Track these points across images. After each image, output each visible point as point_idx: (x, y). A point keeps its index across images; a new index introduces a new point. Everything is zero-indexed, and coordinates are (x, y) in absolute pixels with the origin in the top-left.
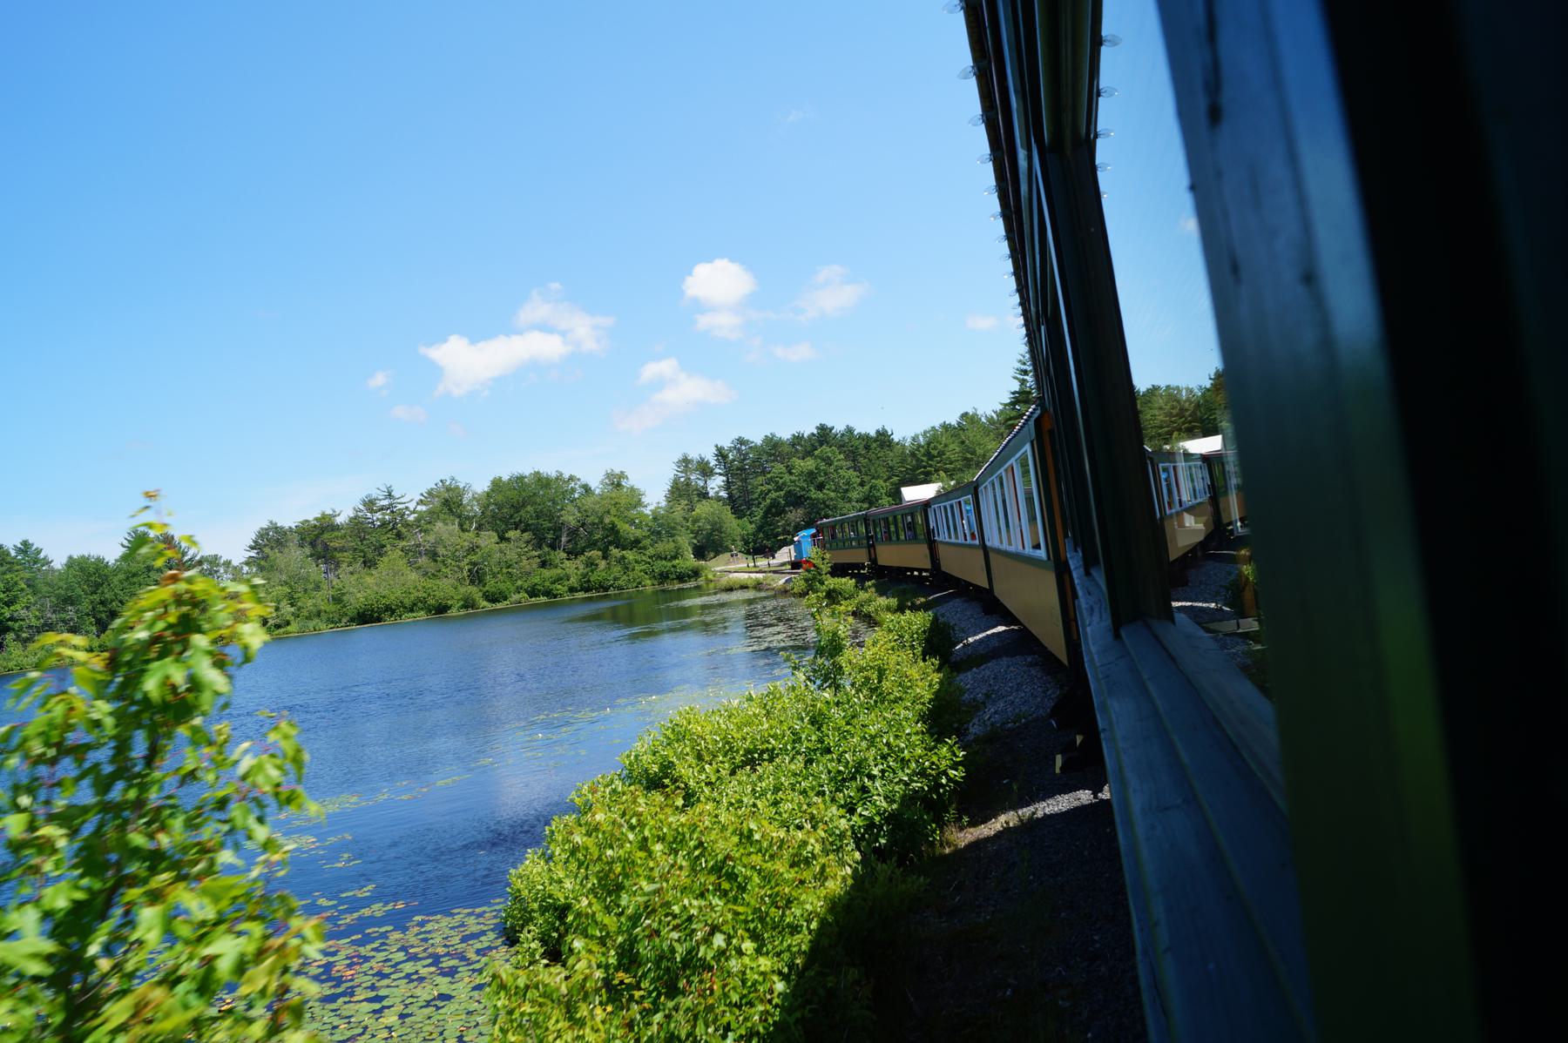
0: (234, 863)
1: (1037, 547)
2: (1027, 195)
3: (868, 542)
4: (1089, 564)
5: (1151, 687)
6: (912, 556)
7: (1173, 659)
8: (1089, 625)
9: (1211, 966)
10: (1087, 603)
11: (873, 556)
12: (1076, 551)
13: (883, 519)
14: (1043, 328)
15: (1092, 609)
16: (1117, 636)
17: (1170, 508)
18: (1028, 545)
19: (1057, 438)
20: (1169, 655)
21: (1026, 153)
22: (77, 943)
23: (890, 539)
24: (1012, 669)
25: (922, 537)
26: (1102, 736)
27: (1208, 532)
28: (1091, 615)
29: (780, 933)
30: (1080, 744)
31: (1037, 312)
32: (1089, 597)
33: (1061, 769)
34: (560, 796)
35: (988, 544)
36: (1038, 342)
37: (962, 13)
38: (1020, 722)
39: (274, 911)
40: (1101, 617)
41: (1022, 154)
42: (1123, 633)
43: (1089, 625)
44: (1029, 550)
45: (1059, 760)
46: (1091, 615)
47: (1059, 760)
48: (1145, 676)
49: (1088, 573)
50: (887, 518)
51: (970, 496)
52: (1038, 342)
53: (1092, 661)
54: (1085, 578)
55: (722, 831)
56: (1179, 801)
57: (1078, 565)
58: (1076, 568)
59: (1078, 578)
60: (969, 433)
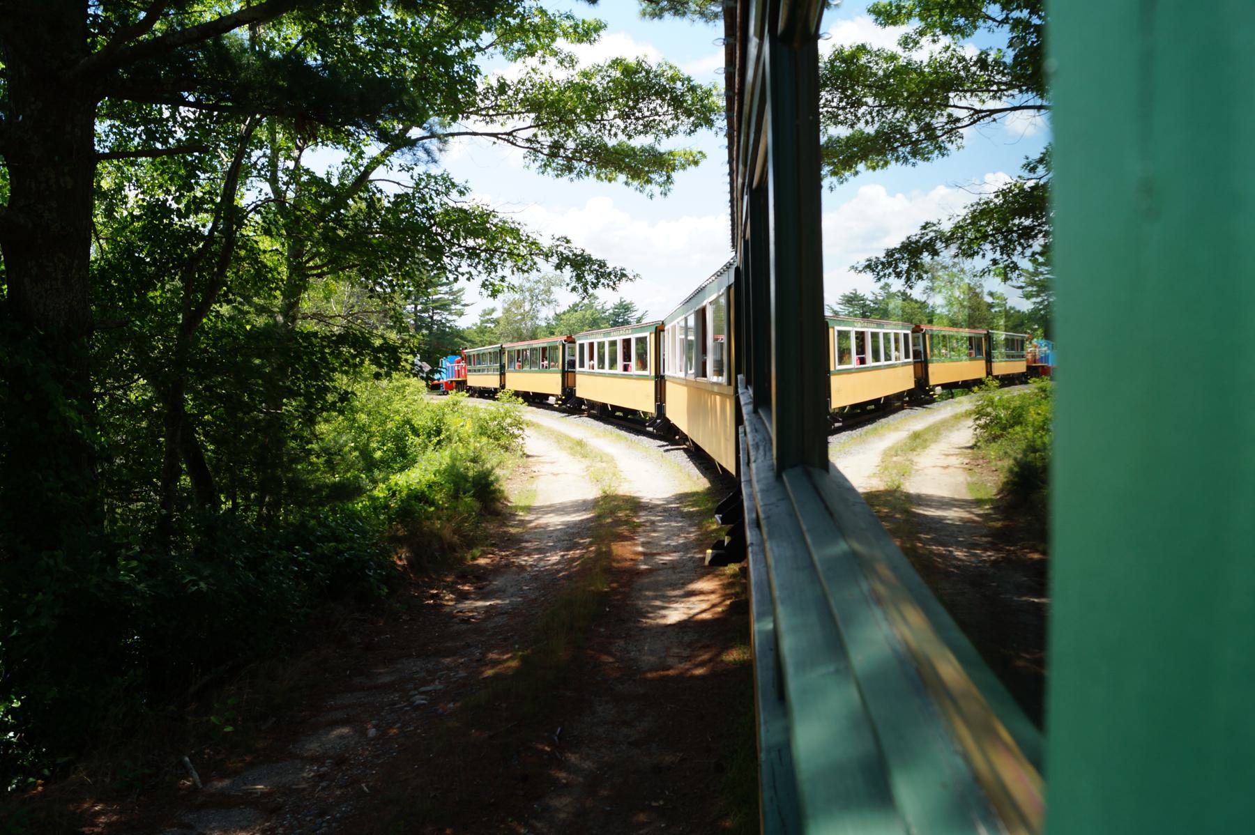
2: (747, 112)
7: (831, 514)
10: (754, 440)
12: (747, 388)
14: (746, 198)
16: (778, 477)
19: (768, 10)
20: (827, 508)
21: (758, 41)
22: (943, 307)
24: (390, 453)
26: (750, 549)
27: (831, 468)
30: (728, 544)
31: (743, 184)
33: (710, 562)
36: (739, 214)
37: (724, 47)
38: (111, 463)
40: (765, 454)
49: (755, 411)
52: (739, 214)
54: (753, 415)
55: (964, 273)
60: (568, 281)
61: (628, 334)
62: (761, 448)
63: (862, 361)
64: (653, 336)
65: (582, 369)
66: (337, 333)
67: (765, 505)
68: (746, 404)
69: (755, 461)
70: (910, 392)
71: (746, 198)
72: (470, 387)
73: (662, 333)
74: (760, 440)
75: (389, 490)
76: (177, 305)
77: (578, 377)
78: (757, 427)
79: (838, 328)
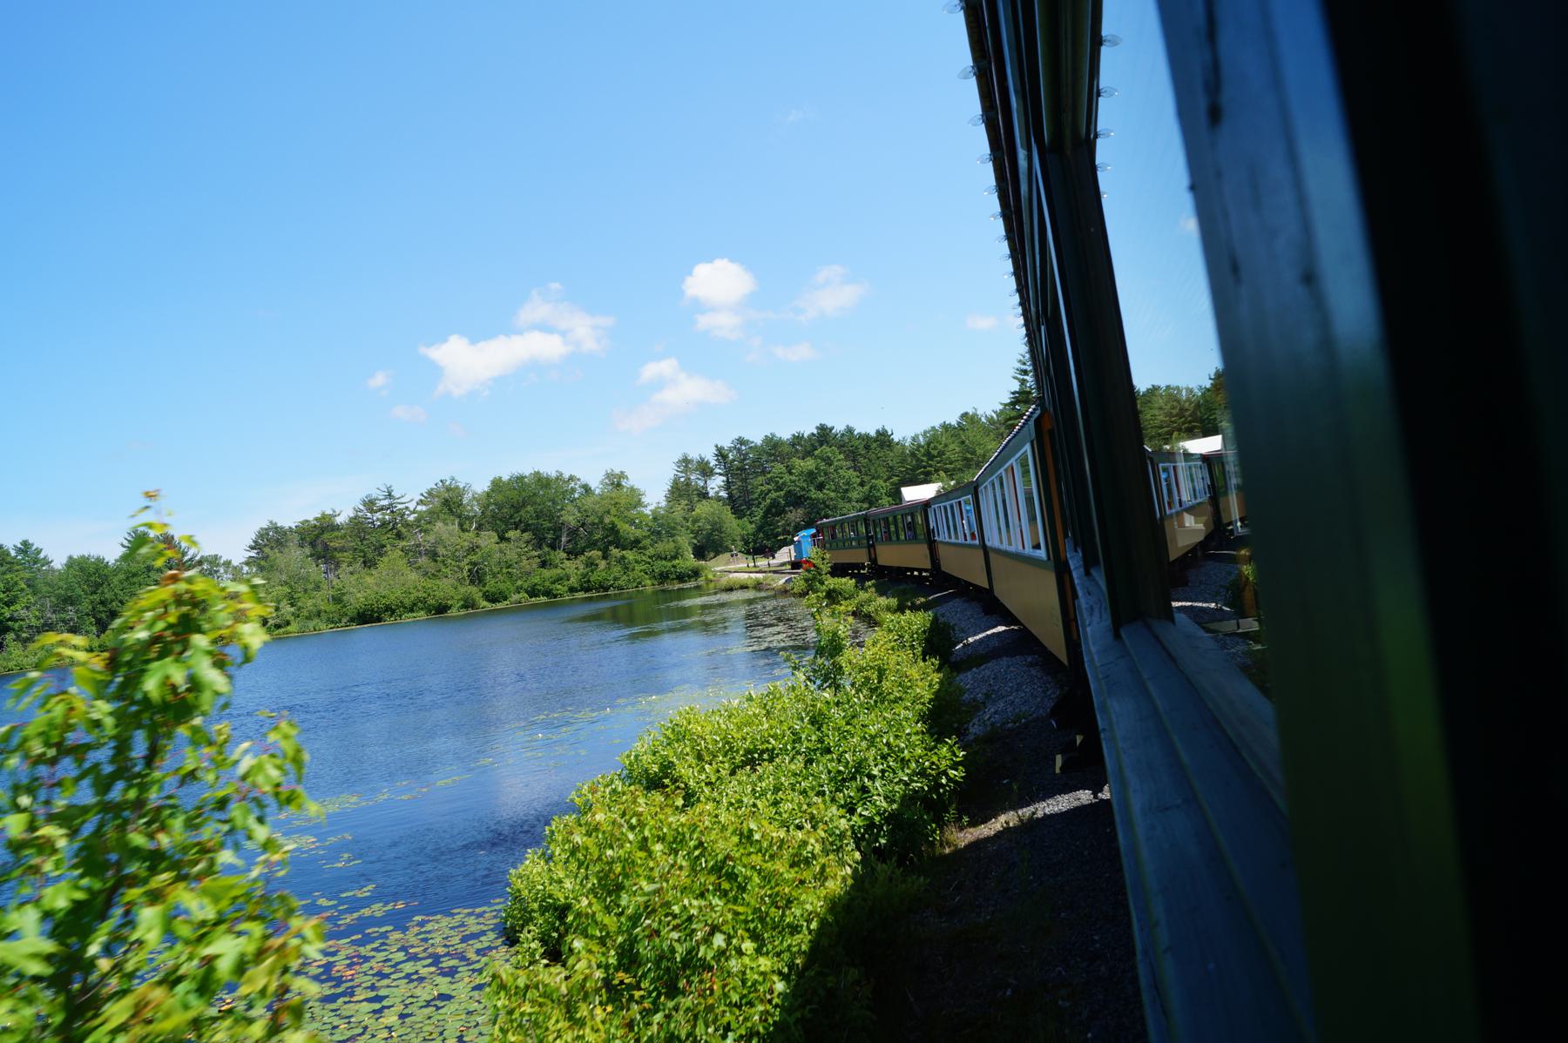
0: (234, 863)
1: (1037, 547)
2: (1027, 195)
3: (868, 542)
5: (1151, 687)
6: (912, 556)
7: (1173, 659)
8: (1089, 625)
9: (1211, 966)
10: (1087, 603)
11: (873, 556)
12: (1076, 551)
13: (883, 519)
14: (1043, 328)
15: (1092, 609)
16: (1117, 636)
18: (1028, 545)
19: (1057, 438)
20: (1169, 655)
21: (1026, 153)
23: (890, 539)
25: (922, 537)
26: (1102, 736)
28: (1091, 615)
30: (1080, 744)
31: (1037, 312)
32: (1089, 597)
33: (1061, 769)
35: (988, 544)
36: (1038, 342)
37: (962, 13)
41: (1022, 154)
42: (1123, 633)
43: (1089, 625)
44: (1029, 550)
45: (1059, 760)
46: (1091, 615)
47: (1059, 760)
48: (1145, 676)
49: (1088, 573)
50: (887, 518)
51: (970, 496)
52: (1038, 342)
54: (1085, 578)
56: (1179, 801)
57: (1078, 565)
58: (1076, 568)
59: (1078, 578)
66: (562, 949)
67: (1102, 666)
75: (560, 796)
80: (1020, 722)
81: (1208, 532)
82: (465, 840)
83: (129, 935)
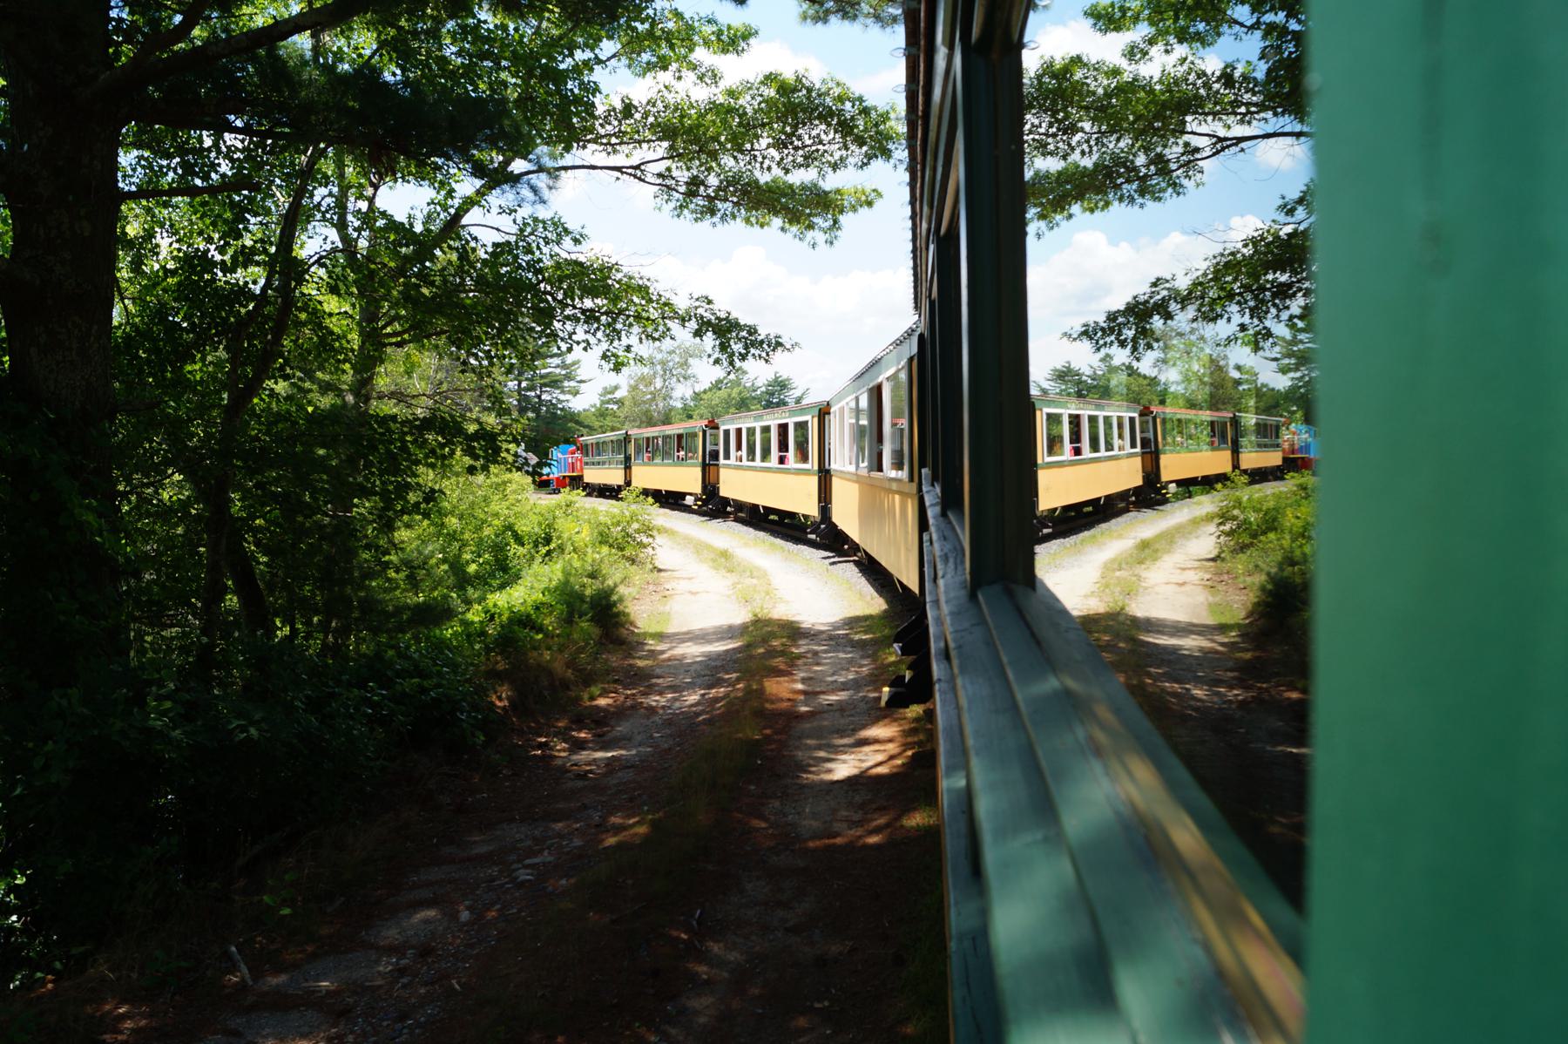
2: (934, 139)
4: (934, 479)
7: (1038, 643)
10: (942, 550)
12: (933, 485)
14: (932, 247)
16: (973, 596)
17: (1051, 451)
20: (1033, 635)
21: (947, 51)
26: (937, 687)
29: (547, 243)
30: (909, 680)
31: (929, 230)
33: (887, 703)
34: (486, 613)
36: (924, 268)
37: (904, 58)
39: (321, 278)
49: (944, 514)
52: (924, 268)
53: (939, 621)
54: (941, 519)
61: (785, 418)
62: (951, 560)
63: (1077, 451)
64: (816, 420)
65: (727, 462)
68: (932, 505)
69: (943, 577)
70: (1137, 491)
71: (932, 247)
72: (587, 484)
73: (827, 417)
74: (950, 550)
76: (221, 382)
77: (722, 471)
78: (946, 533)
79: (1047, 410)
80: (139, 578)
81: (1038, 585)
82: (946, 655)
83: (834, 639)
